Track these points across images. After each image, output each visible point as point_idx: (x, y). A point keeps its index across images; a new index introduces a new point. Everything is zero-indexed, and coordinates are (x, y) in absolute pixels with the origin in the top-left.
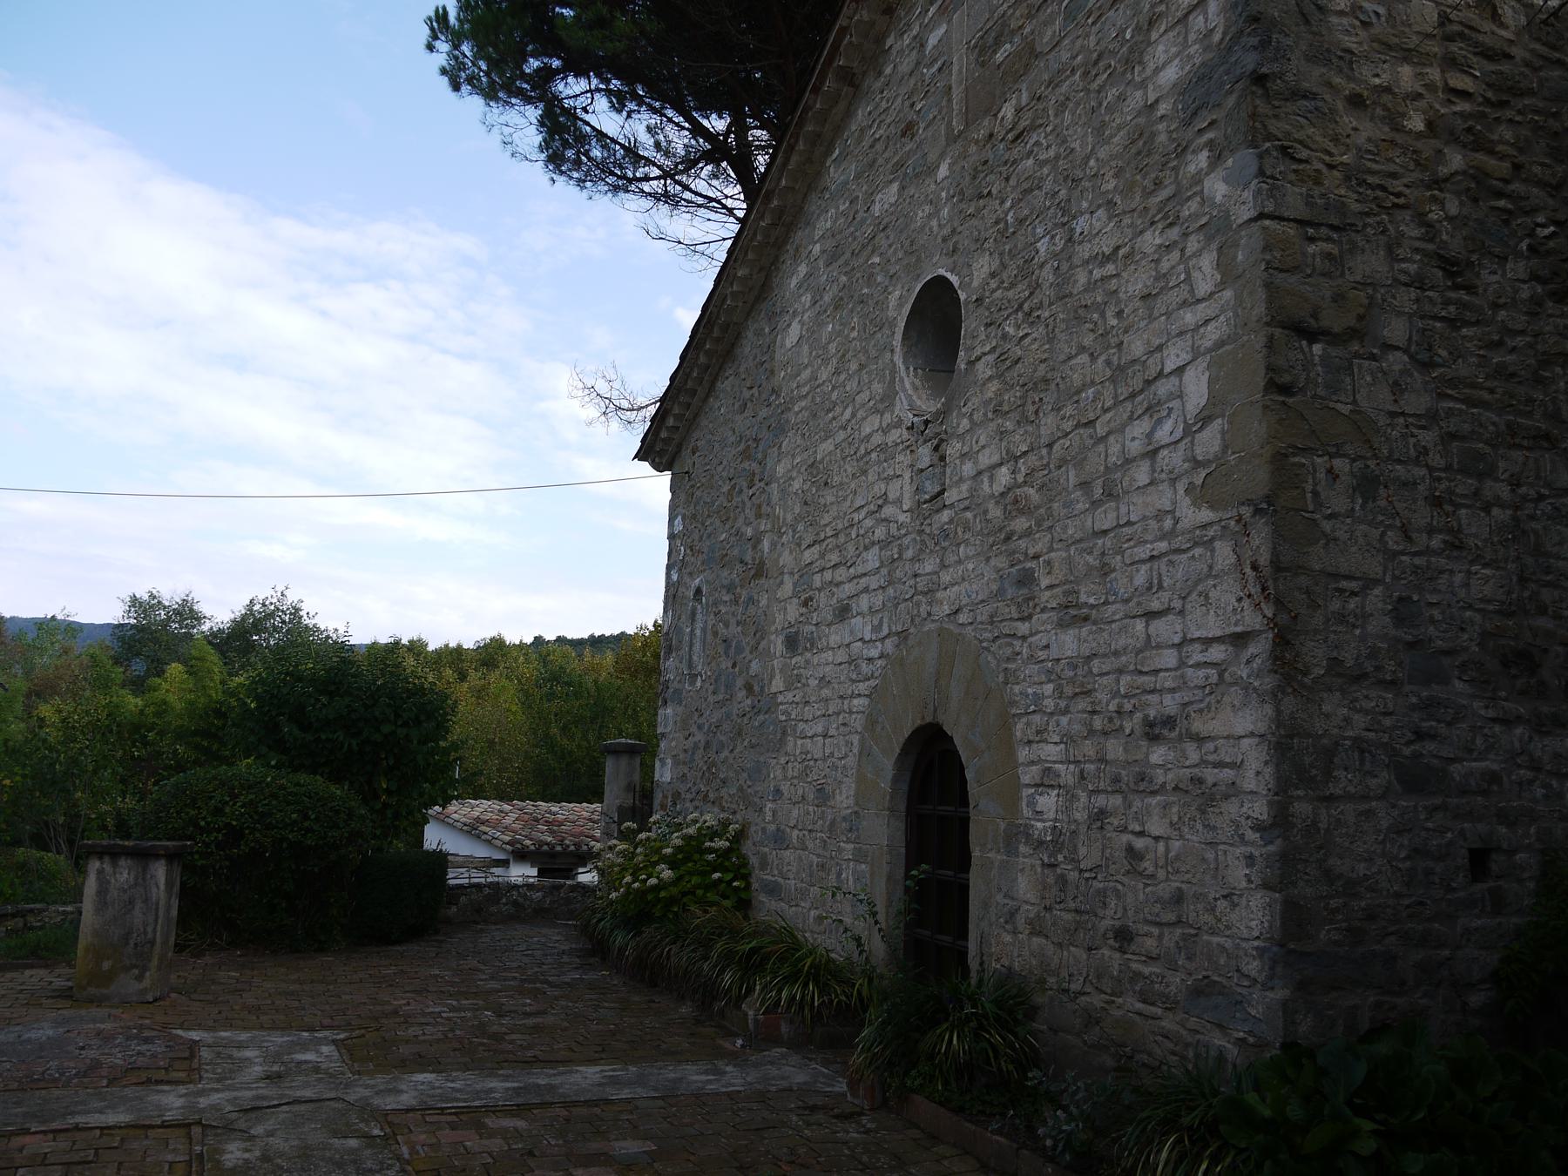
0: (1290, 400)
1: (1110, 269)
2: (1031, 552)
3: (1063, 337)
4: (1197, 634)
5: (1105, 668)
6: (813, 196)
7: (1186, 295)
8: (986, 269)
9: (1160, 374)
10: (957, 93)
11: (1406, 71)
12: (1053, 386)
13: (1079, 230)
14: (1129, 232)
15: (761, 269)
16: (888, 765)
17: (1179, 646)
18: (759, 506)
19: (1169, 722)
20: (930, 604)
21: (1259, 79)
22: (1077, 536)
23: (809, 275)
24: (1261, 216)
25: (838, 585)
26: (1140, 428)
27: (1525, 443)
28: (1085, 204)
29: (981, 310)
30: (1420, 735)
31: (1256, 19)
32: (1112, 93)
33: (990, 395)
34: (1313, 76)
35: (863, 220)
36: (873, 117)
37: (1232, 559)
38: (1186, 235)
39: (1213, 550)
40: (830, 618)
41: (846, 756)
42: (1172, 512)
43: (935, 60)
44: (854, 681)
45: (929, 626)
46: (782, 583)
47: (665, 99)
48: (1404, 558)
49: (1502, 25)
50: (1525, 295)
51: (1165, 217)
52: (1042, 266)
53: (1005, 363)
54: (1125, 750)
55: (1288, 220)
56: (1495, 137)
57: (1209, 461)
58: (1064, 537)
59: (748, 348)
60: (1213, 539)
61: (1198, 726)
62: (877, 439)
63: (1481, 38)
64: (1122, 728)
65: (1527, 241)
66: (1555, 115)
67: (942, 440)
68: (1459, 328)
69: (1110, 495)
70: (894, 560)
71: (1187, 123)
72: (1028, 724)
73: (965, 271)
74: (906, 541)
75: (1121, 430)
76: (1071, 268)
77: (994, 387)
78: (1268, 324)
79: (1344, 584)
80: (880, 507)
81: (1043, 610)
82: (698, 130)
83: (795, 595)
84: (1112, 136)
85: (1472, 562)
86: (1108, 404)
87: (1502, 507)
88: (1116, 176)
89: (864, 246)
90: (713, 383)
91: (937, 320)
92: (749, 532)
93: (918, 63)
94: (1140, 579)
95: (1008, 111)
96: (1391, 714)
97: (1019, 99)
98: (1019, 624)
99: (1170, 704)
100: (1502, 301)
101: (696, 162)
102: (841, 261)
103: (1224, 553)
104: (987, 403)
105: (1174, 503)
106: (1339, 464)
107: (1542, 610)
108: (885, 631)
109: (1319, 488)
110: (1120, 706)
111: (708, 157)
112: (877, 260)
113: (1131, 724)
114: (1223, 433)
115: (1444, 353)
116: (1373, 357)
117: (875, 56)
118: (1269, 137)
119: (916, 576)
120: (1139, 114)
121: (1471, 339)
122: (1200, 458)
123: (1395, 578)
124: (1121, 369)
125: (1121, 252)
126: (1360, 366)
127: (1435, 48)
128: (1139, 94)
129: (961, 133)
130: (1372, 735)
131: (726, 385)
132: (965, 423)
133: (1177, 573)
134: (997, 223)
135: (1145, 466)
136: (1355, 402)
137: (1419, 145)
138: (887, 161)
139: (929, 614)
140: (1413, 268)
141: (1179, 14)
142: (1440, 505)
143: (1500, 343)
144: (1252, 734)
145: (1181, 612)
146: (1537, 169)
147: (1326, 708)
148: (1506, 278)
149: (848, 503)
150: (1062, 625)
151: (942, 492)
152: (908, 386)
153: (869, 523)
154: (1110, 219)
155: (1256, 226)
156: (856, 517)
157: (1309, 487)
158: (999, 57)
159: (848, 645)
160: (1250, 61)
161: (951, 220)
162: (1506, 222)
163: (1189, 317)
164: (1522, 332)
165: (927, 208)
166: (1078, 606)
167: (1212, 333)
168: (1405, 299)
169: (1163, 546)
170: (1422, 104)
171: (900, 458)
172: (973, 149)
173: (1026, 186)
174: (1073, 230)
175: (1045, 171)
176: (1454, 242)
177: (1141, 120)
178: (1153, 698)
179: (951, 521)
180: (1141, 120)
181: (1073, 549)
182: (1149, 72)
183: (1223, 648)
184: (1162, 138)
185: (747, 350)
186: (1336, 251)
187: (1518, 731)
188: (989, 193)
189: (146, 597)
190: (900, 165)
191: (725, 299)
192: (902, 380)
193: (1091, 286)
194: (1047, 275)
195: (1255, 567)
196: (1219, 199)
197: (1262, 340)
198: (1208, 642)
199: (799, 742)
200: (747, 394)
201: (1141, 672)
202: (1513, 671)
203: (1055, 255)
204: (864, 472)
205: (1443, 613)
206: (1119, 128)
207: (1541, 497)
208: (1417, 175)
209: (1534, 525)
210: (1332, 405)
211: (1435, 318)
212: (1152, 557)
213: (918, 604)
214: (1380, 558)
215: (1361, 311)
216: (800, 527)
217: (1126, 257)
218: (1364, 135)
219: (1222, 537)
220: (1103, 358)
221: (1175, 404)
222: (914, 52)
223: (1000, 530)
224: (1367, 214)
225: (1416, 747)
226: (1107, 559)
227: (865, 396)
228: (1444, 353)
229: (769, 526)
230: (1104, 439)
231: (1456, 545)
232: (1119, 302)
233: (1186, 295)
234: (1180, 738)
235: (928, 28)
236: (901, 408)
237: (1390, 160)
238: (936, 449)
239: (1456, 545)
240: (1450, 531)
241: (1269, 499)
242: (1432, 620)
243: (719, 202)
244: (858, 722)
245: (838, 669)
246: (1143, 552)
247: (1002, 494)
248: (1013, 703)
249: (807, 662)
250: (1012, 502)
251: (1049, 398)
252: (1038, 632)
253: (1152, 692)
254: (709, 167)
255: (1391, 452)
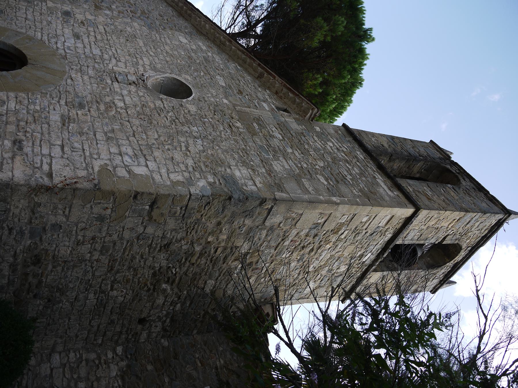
0: (132, 198)
1: (184, 149)
2: (91, 109)
3: (165, 131)
4: (53, 161)
5: (44, 129)
6: (227, 57)
7: (171, 170)
8: (191, 109)
9: (147, 160)
10: (248, 110)
11: (225, 237)
12: (149, 125)
13: (198, 141)
14: (194, 156)
15: (207, 33)
16: (11, 42)
17: (50, 155)
18: (123, 13)
19: (21, 148)
20: (76, 70)
21: (230, 198)
22: (95, 126)
23: (202, 50)
24: (191, 195)
25: (88, 37)
26: (130, 151)
27: (110, 264)
28: (205, 144)
29: (178, 106)
30: (10, 230)
31: (247, 199)
32: (236, 156)
33: (150, 104)
34: (228, 213)
35: (215, 72)
36: (247, 82)
37: (80, 175)
38: (189, 172)
39: (84, 170)
40: (75, 31)
41: (17, 26)
42: (99, 158)
43: (259, 105)
44: (48, 35)
45: (67, 68)
46: (92, 15)
47: (269, 13)
48: (75, 228)
49: (232, 262)
50: (156, 265)
51: (196, 167)
52: (189, 127)
53: (160, 111)
54: (10, 132)
55: (188, 202)
56: (202, 259)
57: (115, 172)
58: (95, 121)
59: (181, 22)
60: (88, 170)
61: (18, 158)
62: (141, 62)
63: (230, 256)
64: (20, 132)
65: (172, 266)
66: (206, 274)
67: (137, 85)
68: (148, 247)
69: (108, 139)
70: (95, 60)
71: (222, 177)
72: (24, 98)
73: (192, 102)
74: (102, 65)
75: (130, 145)
76: (186, 137)
77: (152, 106)
78: (157, 194)
79: (68, 209)
80: (116, 58)
81: (69, 110)
82: (258, 22)
83: (86, 19)
84: (224, 155)
85: (72, 247)
86: (140, 142)
87: (90, 257)
88: (212, 154)
89: (207, 71)
90: (171, 6)
91: (178, 90)
92: (114, 7)
93: (259, 99)
94: (76, 145)
95: (239, 124)
96: (19, 221)
97: (241, 128)
98: (65, 101)
99: (27, 149)
100: (155, 259)
101: (248, 18)
102: (204, 62)
103: (82, 173)
104: (147, 102)
105: (102, 159)
106: (110, 210)
107: (54, 267)
108: (67, 51)
109: (101, 204)
110: (28, 132)
111: (249, 23)
112: (202, 74)
113: (21, 135)
114: (124, 177)
115: (141, 243)
116: (142, 223)
117: (265, 86)
118: (213, 199)
119: (88, 67)
120: (228, 163)
121: (145, 250)
122: (117, 169)
123: (68, 225)
124: (151, 148)
125: (188, 153)
126: (140, 219)
127: (230, 245)
128: (234, 164)
129: (236, 109)
130: (11, 214)
131: (170, 10)
132: (141, 94)
133: (77, 157)
134: (205, 115)
135: (117, 151)
136: (129, 217)
137: (204, 239)
138: (233, 84)
139: (72, 69)
140: (168, 236)
141: (254, 178)
142: (92, 239)
143: (142, 258)
144: (13, 176)
145: (62, 157)
146: (192, 269)
147: (22, 201)
148: (162, 260)
149: (119, 47)
150: (62, 116)
151: (118, 82)
152: (158, 77)
153: (110, 53)
154: (199, 151)
155: (188, 193)
156: (113, 49)
157: (102, 201)
158: (255, 124)
159: (63, 36)
160: (236, 196)
161: (209, 101)
162: (178, 261)
163: (163, 171)
164: (145, 264)
165: (215, 94)
166: (69, 122)
167: (157, 177)
168: (159, 233)
169: (87, 154)
170: (215, 240)
171: (133, 69)
172: (230, 112)
173: (215, 126)
174: (198, 139)
175: (218, 133)
176: (173, 247)
177: (226, 164)
178: (30, 144)
179: (107, 83)
180: (226, 164)
181: (91, 124)
182: (240, 167)
183: (48, 169)
184: (220, 169)
185: (181, 22)
186: (177, 215)
187: (11, 259)
188: (215, 115)
189: (365, 62)
190: (230, 87)
191: (199, 18)
192: (160, 75)
193: (179, 142)
194: (186, 129)
195: (76, 182)
196: (198, 183)
197: (152, 192)
198: (50, 165)
199: (24, 8)
200: (165, 18)
201: (41, 141)
202: (33, 258)
203: (191, 132)
204: (129, 55)
205: (55, 238)
206: (226, 157)
207: (92, 268)
208: (195, 238)
209: (83, 266)
210: (129, 210)
211: (152, 241)
212: (84, 150)
213: (77, 66)
214: (76, 221)
215: (157, 221)
216: (112, 27)
217: (186, 154)
218: (209, 225)
219: (88, 173)
220: (155, 143)
221: (136, 163)
222: (262, 98)
223: (101, 100)
224: (186, 224)
225: (6, 228)
226: (85, 135)
227: (157, 61)
228: (141, 243)
229: (114, 15)
230: (128, 139)
231: (78, 243)
232: (172, 150)
233: (171, 170)
234: (13, 152)
235: (269, 105)
236: (150, 73)
237: (201, 231)
238: (134, 82)
239: (78, 243)
240: (83, 242)
241: (99, 189)
242: (52, 235)
243: (234, 24)
244: (31, 33)
245: (54, 30)
246: (86, 147)
247: (114, 103)
248: (33, 94)
249: (58, 18)
250: (110, 105)
251: (145, 124)
252: (60, 107)
253: (33, 144)
254: (246, 23)
255: (111, 226)
